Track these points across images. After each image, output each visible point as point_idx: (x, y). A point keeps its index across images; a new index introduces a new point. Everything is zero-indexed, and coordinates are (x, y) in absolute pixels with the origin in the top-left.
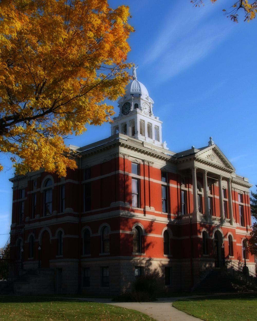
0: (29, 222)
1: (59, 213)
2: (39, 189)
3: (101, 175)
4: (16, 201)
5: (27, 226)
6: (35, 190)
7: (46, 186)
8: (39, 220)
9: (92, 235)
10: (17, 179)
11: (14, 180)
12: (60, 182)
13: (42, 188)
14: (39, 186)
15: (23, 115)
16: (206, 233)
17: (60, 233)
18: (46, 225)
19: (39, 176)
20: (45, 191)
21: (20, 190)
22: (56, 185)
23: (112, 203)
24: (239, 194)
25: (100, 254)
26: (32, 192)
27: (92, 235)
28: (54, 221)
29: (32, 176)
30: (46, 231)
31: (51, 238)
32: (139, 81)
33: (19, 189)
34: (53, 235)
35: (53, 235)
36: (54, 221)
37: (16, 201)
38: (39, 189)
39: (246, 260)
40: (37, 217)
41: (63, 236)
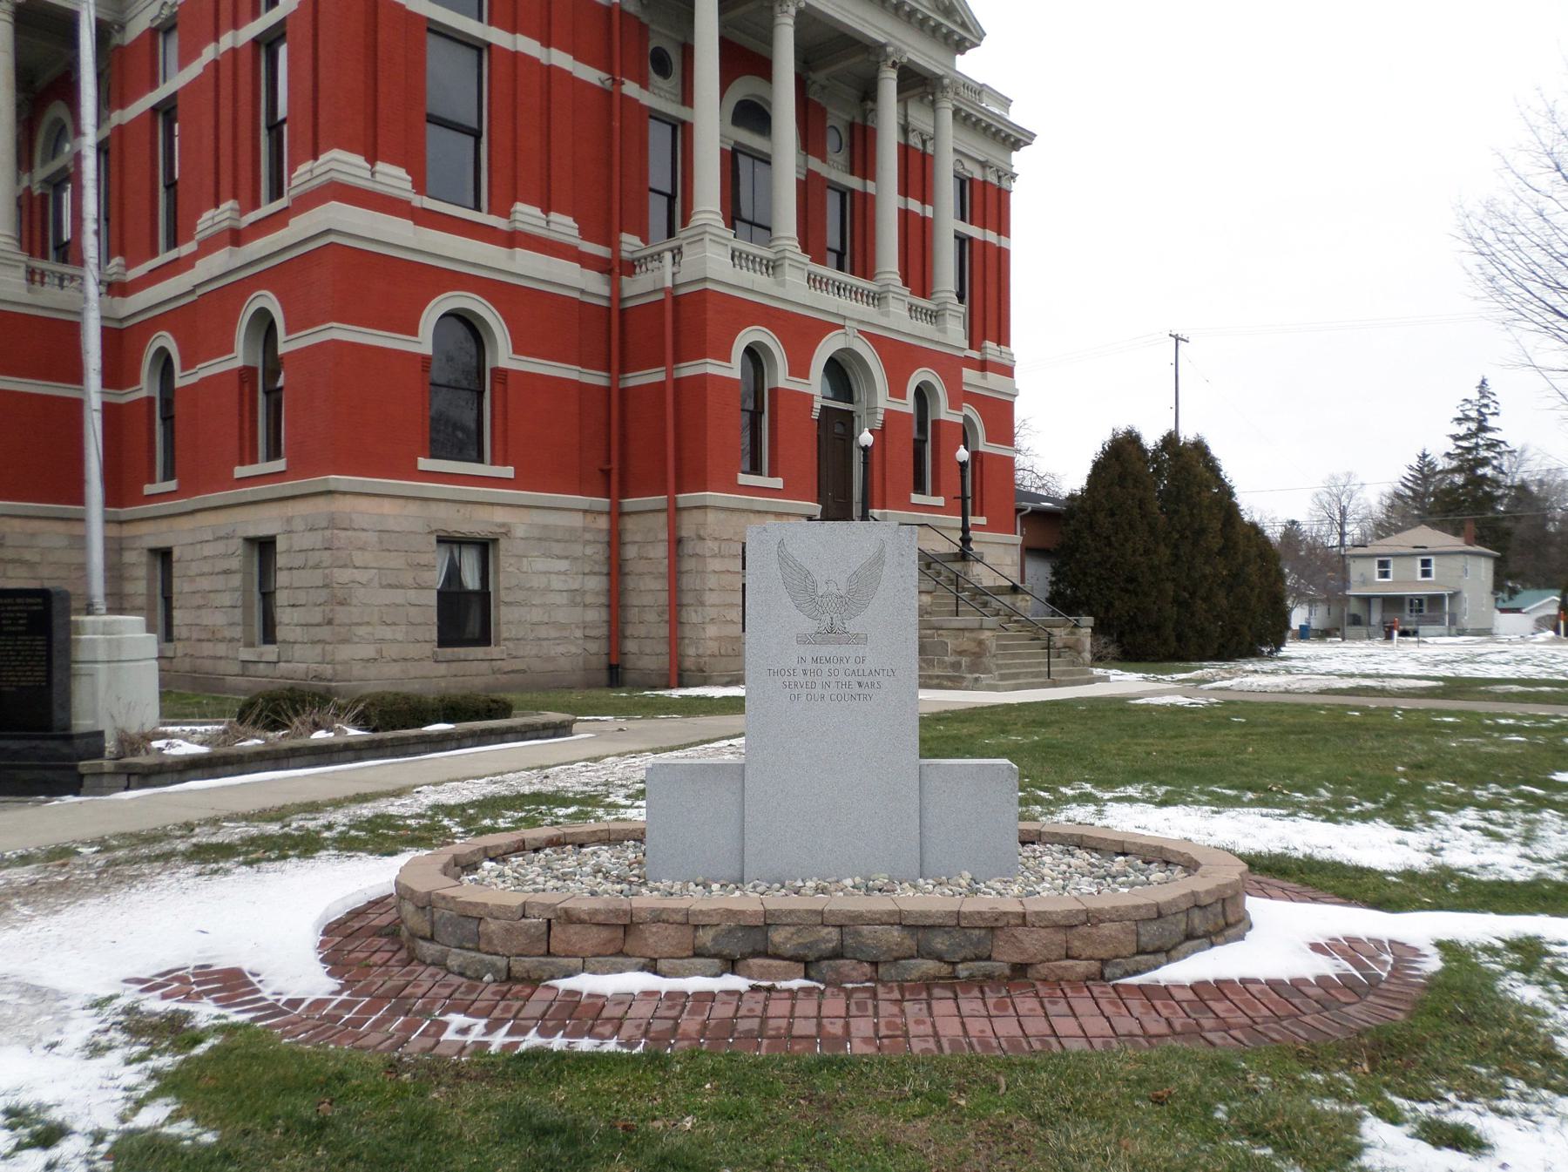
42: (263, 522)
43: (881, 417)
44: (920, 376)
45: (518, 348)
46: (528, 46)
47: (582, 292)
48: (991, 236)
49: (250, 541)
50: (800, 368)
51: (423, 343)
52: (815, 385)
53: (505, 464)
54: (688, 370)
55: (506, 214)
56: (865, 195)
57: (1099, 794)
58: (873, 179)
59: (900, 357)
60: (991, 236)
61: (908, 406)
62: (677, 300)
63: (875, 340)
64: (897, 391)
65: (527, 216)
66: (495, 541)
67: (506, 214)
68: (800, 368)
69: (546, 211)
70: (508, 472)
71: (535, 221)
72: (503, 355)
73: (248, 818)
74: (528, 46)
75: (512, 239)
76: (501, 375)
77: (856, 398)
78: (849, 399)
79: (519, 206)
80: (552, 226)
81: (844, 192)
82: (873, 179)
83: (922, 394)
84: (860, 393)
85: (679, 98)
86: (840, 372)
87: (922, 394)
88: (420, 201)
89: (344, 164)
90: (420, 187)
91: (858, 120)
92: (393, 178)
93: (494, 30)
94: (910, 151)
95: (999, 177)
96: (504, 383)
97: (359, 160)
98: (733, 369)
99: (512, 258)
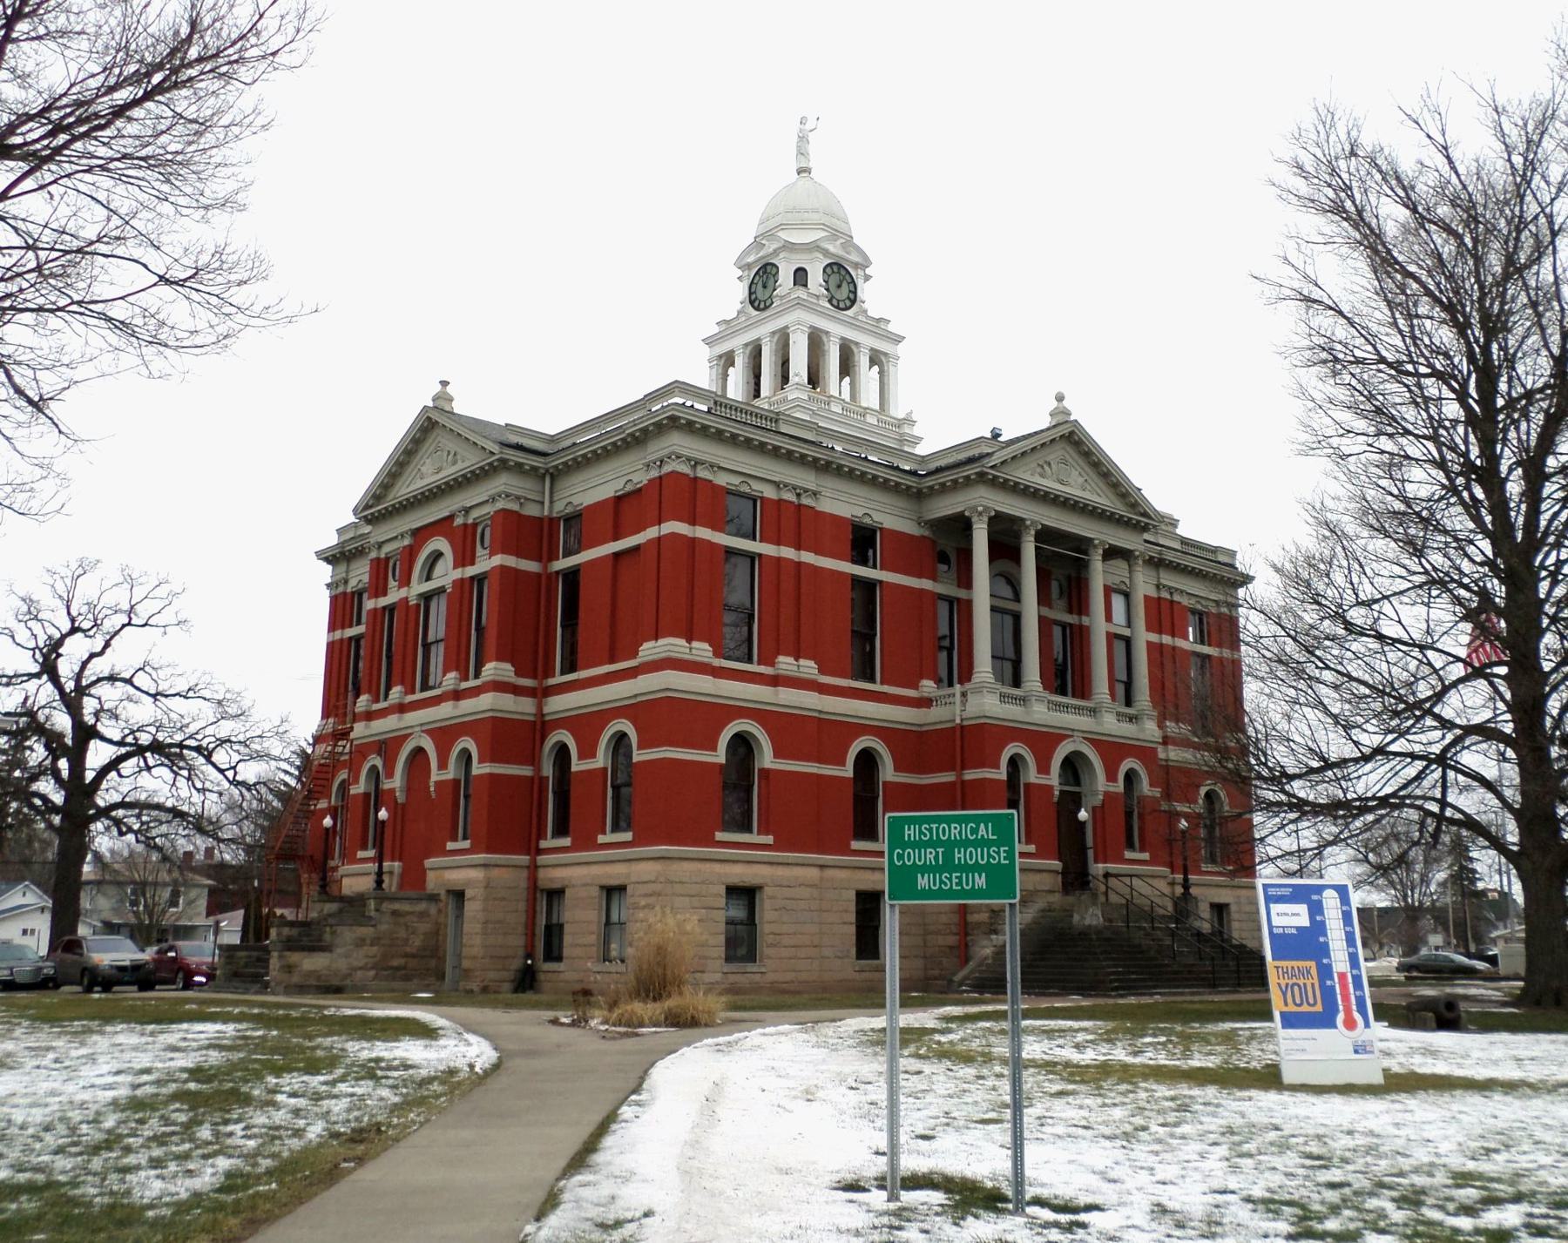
0: (369, 716)
1: (413, 692)
2: (403, 593)
3: (616, 538)
4: (338, 634)
5: (360, 730)
6: (394, 595)
7: (428, 578)
8: (402, 708)
9: (577, 765)
10: (342, 553)
11: (334, 556)
12: (472, 563)
13: (418, 588)
14: (406, 581)
15: (1519, 536)
16: (12, 1201)
17: (466, 756)
18: (421, 725)
19: (407, 542)
20: (427, 597)
21: (353, 593)
22: (458, 574)
23: (646, 645)
24: (1194, 612)
25: (601, 839)
26: (383, 602)
27: (638, 756)
28: (446, 711)
29: (383, 542)
30: (419, 752)
31: (436, 776)
32: (1538, 526)
33: (349, 590)
34: (443, 765)
35: (443, 765)
36: (446, 711)
37: (338, 634)
38: (403, 593)
39: (1192, 878)
40: (396, 692)
41: (478, 769)
42: (615, 874)
43: (1101, 797)
44: (1128, 764)
45: (778, 754)
46: (788, 553)
47: (820, 712)
48: (1226, 653)
49: (602, 887)
50: (1044, 768)
51: (720, 756)
52: (1054, 779)
53: (767, 834)
54: (970, 775)
55: (772, 664)
56: (1081, 627)
57: (54, 1044)
58: (1087, 614)
59: (1112, 751)
60: (1226, 653)
61: (1119, 787)
62: (962, 727)
63: (1096, 743)
64: (1111, 777)
65: (785, 664)
66: (760, 888)
67: (772, 664)
68: (1044, 768)
69: (689, 641)
70: (769, 839)
71: (790, 667)
72: (767, 759)
73: (116, 1033)
74: (788, 553)
75: (775, 681)
76: (765, 773)
77: (1082, 782)
78: (1078, 783)
79: (781, 658)
80: (694, 651)
81: (1064, 626)
82: (1087, 614)
83: (1130, 777)
84: (1085, 779)
85: (955, 582)
86: (1073, 767)
87: (1130, 777)
88: (718, 662)
89: (672, 646)
90: (717, 654)
91: (1074, 575)
92: (702, 650)
93: (884, 572)
94: (1175, 607)
95: (798, 495)
96: (767, 778)
97: (683, 642)
98: (1002, 774)
99: (777, 694)
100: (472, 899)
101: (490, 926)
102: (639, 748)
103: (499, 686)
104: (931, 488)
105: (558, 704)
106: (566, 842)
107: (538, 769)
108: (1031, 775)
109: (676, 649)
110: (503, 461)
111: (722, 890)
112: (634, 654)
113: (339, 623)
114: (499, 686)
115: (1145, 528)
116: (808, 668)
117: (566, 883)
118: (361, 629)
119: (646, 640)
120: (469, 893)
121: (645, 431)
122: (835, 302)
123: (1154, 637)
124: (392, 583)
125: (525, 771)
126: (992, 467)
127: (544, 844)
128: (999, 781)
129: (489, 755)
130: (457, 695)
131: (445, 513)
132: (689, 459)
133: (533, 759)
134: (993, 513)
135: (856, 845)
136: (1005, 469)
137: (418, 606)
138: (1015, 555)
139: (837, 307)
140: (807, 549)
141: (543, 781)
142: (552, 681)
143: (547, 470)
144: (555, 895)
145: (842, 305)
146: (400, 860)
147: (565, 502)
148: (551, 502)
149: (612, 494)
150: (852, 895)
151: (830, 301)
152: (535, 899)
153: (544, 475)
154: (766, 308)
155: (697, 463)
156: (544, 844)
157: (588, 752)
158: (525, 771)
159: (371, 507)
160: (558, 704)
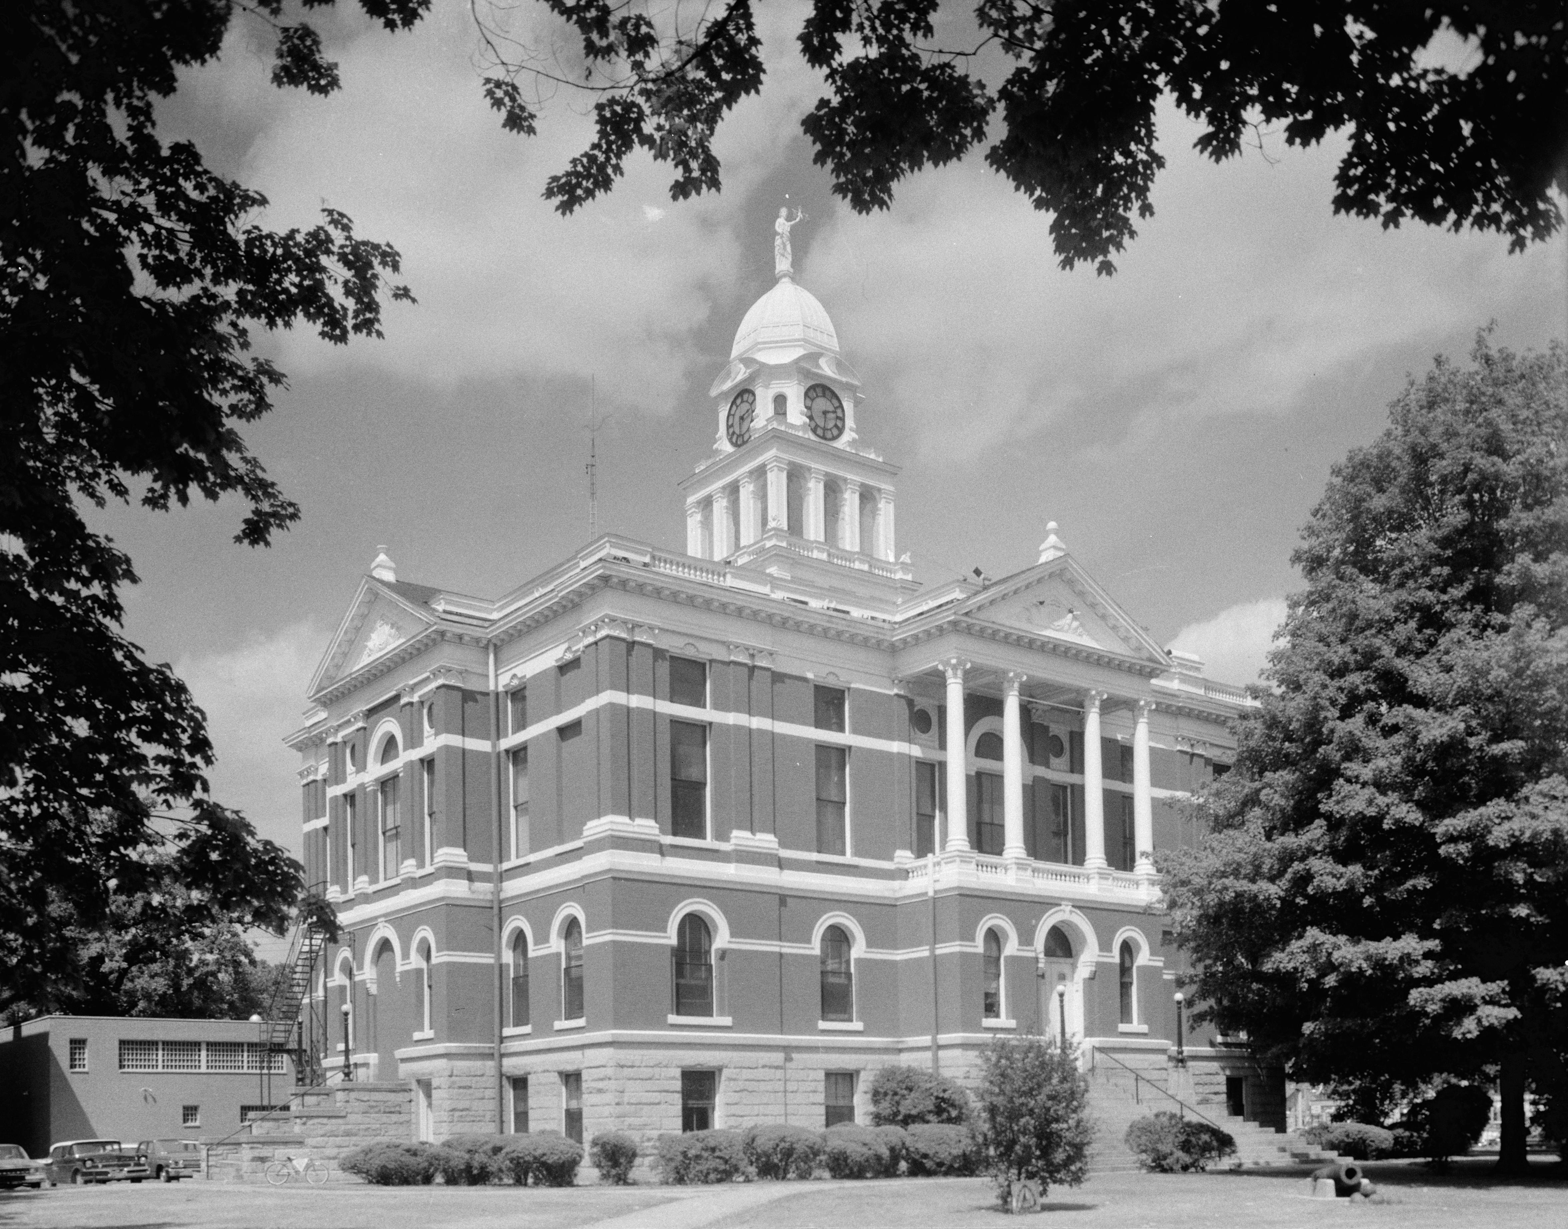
9: (533, 951)
14: (361, 767)
23: (590, 824)
31: (400, 967)
35: (406, 955)
49: (560, 1073)
50: (1026, 938)
64: (1105, 946)
65: (740, 838)
68: (1026, 938)
95: (752, 656)
97: (626, 819)
100: (439, 1088)
101: (457, 1114)
102: (590, 929)
103: (451, 872)
104: (904, 641)
105: (513, 887)
106: (527, 1029)
107: (499, 956)
108: (1011, 947)
109: (620, 827)
110: (443, 634)
111: (821, 1075)
112: (578, 834)
113: (312, 813)
114: (451, 872)
115: (1152, 674)
116: (766, 841)
117: (528, 1069)
118: (324, 821)
119: (590, 819)
120: (435, 1083)
121: (579, 594)
122: (820, 432)
123: (1163, 794)
124: (350, 768)
125: (486, 959)
126: (966, 614)
127: (507, 1031)
128: (975, 954)
129: (450, 942)
130: (414, 883)
131: (393, 693)
132: (625, 622)
133: (492, 947)
134: (968, 666)
135: (822, 1025)
136: (982, 615)
137: (375, 791)
138: (995, 707)
139: (824, 437)
140: (473, 736)
141: (502, 968)
142: (506, 866)
143: (489, 641)
144: (520, 1083)
145: (829, 435)
146: (376, 1051)
147: (510, 674)
148: (497, 676)
149: (554, 664)
150: (677, 1073)
151: (814, 431)
152: (501, 1086)
153: (486, 648)
154: (744, 443)
155: (636, 626)
156: (507, 1031)
157: (542, 938)
158: (486, 959)
159: (324, 689)
160: (513, 887)
